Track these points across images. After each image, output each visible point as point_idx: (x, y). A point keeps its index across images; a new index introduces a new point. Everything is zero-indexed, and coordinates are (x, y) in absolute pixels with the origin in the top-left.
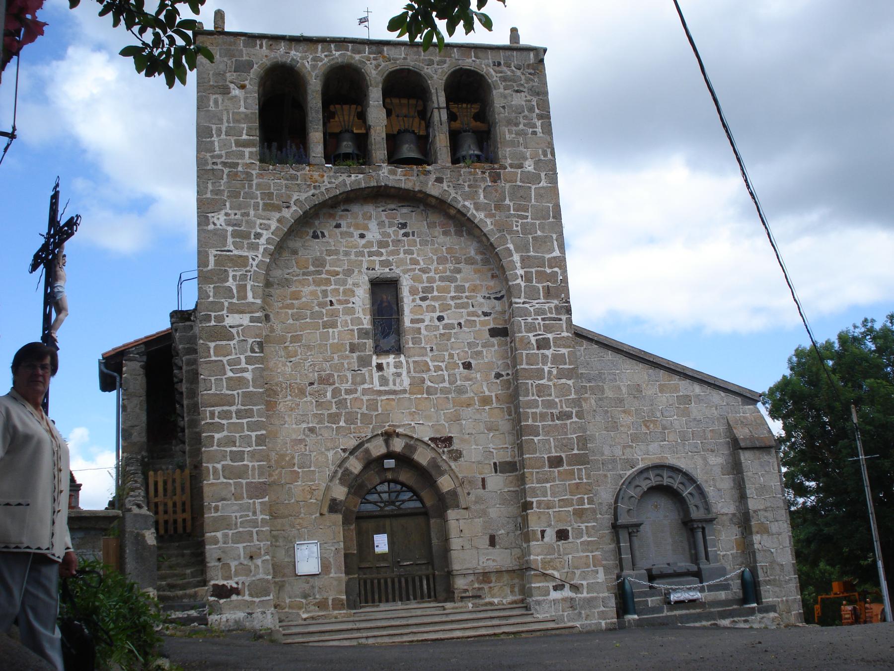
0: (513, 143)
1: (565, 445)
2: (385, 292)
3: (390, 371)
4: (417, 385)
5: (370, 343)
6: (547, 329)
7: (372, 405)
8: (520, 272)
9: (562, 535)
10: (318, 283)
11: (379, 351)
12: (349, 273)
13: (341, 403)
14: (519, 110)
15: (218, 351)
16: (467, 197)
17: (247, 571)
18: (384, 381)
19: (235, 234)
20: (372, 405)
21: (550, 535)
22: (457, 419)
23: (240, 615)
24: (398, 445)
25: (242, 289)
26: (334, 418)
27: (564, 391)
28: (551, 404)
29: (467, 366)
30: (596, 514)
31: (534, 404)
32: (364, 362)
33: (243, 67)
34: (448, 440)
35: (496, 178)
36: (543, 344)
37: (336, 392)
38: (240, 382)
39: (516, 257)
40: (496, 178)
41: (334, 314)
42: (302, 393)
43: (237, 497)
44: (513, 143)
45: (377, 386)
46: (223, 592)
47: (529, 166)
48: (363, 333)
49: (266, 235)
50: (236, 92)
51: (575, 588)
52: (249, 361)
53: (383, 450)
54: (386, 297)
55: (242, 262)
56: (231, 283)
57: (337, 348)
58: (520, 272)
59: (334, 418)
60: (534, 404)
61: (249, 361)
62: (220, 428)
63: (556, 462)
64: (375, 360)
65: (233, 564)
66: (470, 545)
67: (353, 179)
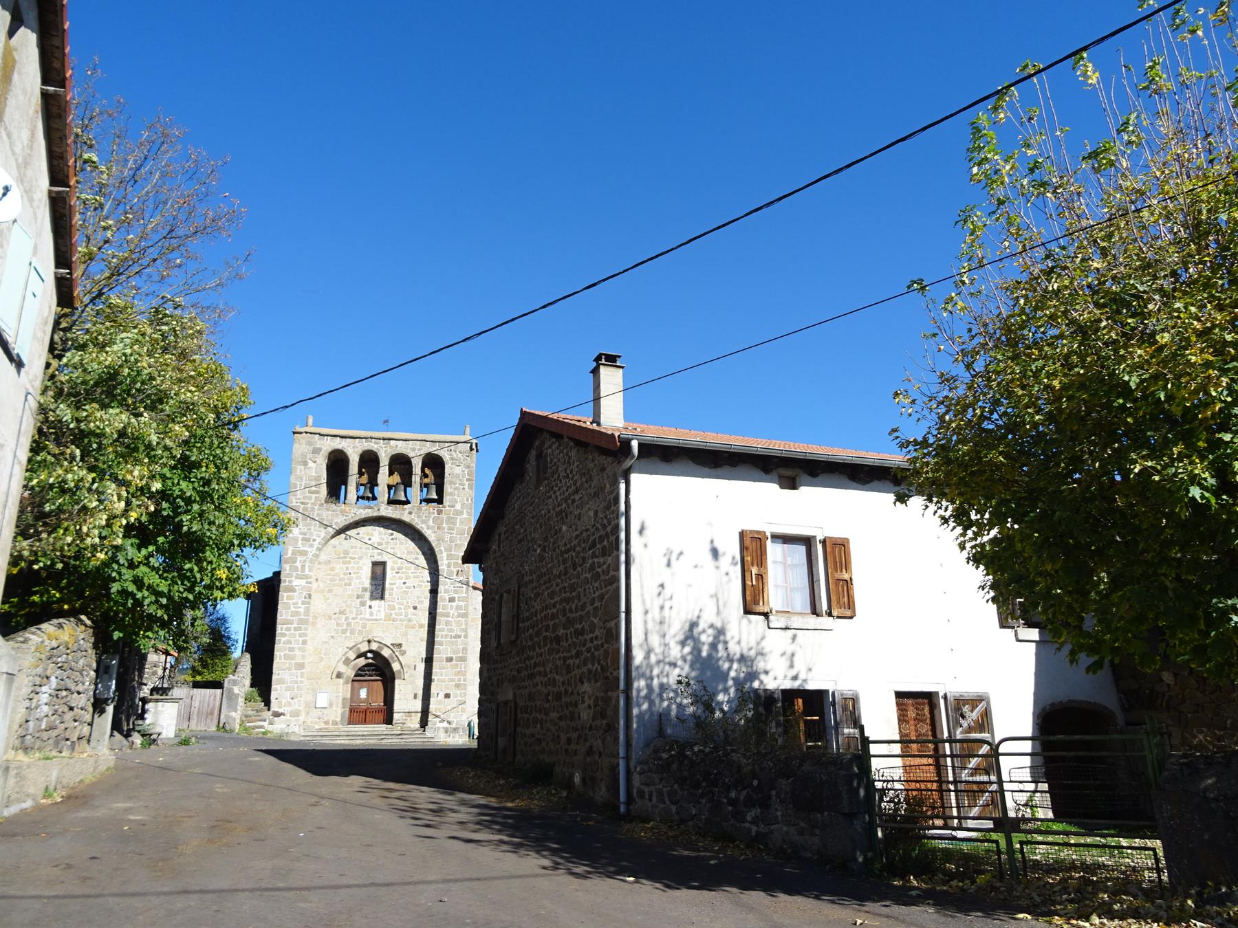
0: (451, 494)
1: (456, 652)
2: (379, 569)
3: (374, 609)
4: (388, 617)
5: (368, 594)
6: (455, 592)
7: (364, 626)
8: (445, 562)
9: (447, 696)
10: (344, 563)
11: (373, 598)
12: (360, 558)
13: (349, 624)
14: (457, 476)
15: (288, 598)
16: (424, 522)
17: (290, 704)
18: (371, 614)
19: (303, 539)
20: (364, 626)
21: (442, 695)
22: (406, 635)
23: (283, 726)
24: (374, 647)
25: (303, 567)
26: (344, 631)
27: (458, 623)
28: (452, 630)
29: (415, 608)
30: (1104, 641)
31: (443, 630)
32: (363, 604)
33: (316, 451)
34: (400, 645)
35: (440, 512)
36: (452, 600)
37: (347, 619)
38: (297, 613)
39: (445, 554)
40: (440, 512)
41: (350, 579)
42: (330, 618)
43: (290, 669)
44: (451, 494)
45: (368, 616)
46: (277, 715)
47: (458, 507)
48: (365, 590)
49: (318, 540)
50: (311, 464)
51: (449, 723)
52: (303, 603)
53: (367, 649)
54: (379, 569)
55: (304, 553)
56: (298, 564)
57: (350, 596)
58: (445, 562)
59: (344, 631)
60: (443, 630)
61: (303, 603)
62: (284, 635)
63: (450, 660)
64: (369, 603)
65: (284, 701)
66: (406, 698)
67: (364, 512)
